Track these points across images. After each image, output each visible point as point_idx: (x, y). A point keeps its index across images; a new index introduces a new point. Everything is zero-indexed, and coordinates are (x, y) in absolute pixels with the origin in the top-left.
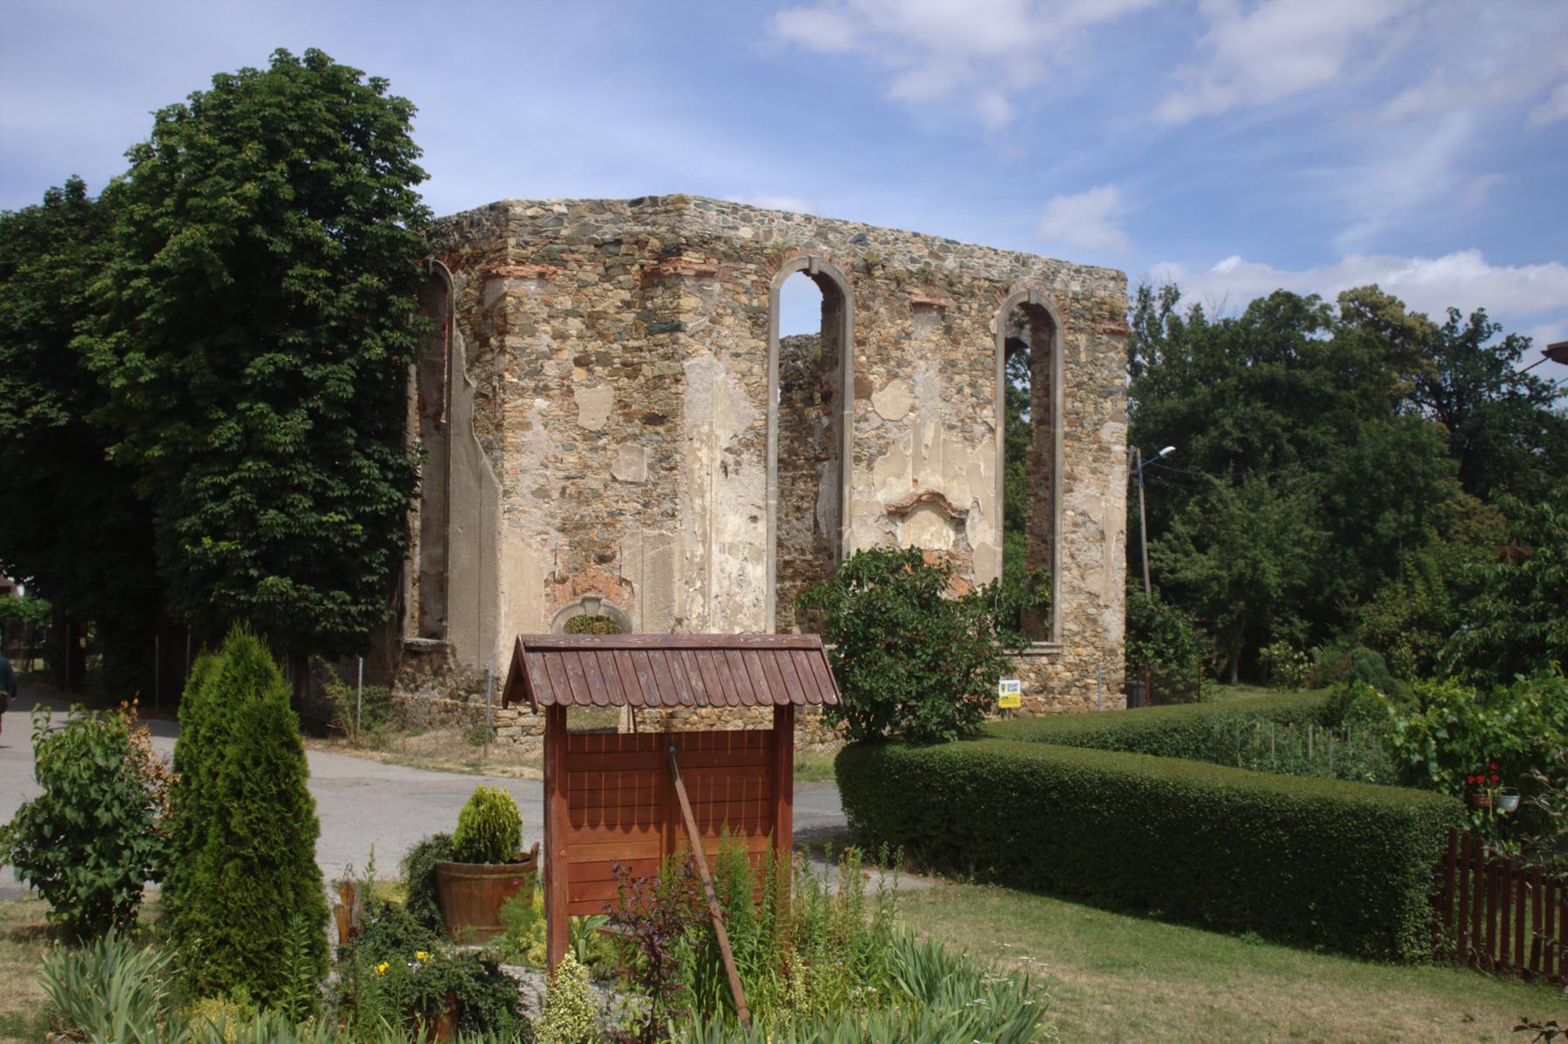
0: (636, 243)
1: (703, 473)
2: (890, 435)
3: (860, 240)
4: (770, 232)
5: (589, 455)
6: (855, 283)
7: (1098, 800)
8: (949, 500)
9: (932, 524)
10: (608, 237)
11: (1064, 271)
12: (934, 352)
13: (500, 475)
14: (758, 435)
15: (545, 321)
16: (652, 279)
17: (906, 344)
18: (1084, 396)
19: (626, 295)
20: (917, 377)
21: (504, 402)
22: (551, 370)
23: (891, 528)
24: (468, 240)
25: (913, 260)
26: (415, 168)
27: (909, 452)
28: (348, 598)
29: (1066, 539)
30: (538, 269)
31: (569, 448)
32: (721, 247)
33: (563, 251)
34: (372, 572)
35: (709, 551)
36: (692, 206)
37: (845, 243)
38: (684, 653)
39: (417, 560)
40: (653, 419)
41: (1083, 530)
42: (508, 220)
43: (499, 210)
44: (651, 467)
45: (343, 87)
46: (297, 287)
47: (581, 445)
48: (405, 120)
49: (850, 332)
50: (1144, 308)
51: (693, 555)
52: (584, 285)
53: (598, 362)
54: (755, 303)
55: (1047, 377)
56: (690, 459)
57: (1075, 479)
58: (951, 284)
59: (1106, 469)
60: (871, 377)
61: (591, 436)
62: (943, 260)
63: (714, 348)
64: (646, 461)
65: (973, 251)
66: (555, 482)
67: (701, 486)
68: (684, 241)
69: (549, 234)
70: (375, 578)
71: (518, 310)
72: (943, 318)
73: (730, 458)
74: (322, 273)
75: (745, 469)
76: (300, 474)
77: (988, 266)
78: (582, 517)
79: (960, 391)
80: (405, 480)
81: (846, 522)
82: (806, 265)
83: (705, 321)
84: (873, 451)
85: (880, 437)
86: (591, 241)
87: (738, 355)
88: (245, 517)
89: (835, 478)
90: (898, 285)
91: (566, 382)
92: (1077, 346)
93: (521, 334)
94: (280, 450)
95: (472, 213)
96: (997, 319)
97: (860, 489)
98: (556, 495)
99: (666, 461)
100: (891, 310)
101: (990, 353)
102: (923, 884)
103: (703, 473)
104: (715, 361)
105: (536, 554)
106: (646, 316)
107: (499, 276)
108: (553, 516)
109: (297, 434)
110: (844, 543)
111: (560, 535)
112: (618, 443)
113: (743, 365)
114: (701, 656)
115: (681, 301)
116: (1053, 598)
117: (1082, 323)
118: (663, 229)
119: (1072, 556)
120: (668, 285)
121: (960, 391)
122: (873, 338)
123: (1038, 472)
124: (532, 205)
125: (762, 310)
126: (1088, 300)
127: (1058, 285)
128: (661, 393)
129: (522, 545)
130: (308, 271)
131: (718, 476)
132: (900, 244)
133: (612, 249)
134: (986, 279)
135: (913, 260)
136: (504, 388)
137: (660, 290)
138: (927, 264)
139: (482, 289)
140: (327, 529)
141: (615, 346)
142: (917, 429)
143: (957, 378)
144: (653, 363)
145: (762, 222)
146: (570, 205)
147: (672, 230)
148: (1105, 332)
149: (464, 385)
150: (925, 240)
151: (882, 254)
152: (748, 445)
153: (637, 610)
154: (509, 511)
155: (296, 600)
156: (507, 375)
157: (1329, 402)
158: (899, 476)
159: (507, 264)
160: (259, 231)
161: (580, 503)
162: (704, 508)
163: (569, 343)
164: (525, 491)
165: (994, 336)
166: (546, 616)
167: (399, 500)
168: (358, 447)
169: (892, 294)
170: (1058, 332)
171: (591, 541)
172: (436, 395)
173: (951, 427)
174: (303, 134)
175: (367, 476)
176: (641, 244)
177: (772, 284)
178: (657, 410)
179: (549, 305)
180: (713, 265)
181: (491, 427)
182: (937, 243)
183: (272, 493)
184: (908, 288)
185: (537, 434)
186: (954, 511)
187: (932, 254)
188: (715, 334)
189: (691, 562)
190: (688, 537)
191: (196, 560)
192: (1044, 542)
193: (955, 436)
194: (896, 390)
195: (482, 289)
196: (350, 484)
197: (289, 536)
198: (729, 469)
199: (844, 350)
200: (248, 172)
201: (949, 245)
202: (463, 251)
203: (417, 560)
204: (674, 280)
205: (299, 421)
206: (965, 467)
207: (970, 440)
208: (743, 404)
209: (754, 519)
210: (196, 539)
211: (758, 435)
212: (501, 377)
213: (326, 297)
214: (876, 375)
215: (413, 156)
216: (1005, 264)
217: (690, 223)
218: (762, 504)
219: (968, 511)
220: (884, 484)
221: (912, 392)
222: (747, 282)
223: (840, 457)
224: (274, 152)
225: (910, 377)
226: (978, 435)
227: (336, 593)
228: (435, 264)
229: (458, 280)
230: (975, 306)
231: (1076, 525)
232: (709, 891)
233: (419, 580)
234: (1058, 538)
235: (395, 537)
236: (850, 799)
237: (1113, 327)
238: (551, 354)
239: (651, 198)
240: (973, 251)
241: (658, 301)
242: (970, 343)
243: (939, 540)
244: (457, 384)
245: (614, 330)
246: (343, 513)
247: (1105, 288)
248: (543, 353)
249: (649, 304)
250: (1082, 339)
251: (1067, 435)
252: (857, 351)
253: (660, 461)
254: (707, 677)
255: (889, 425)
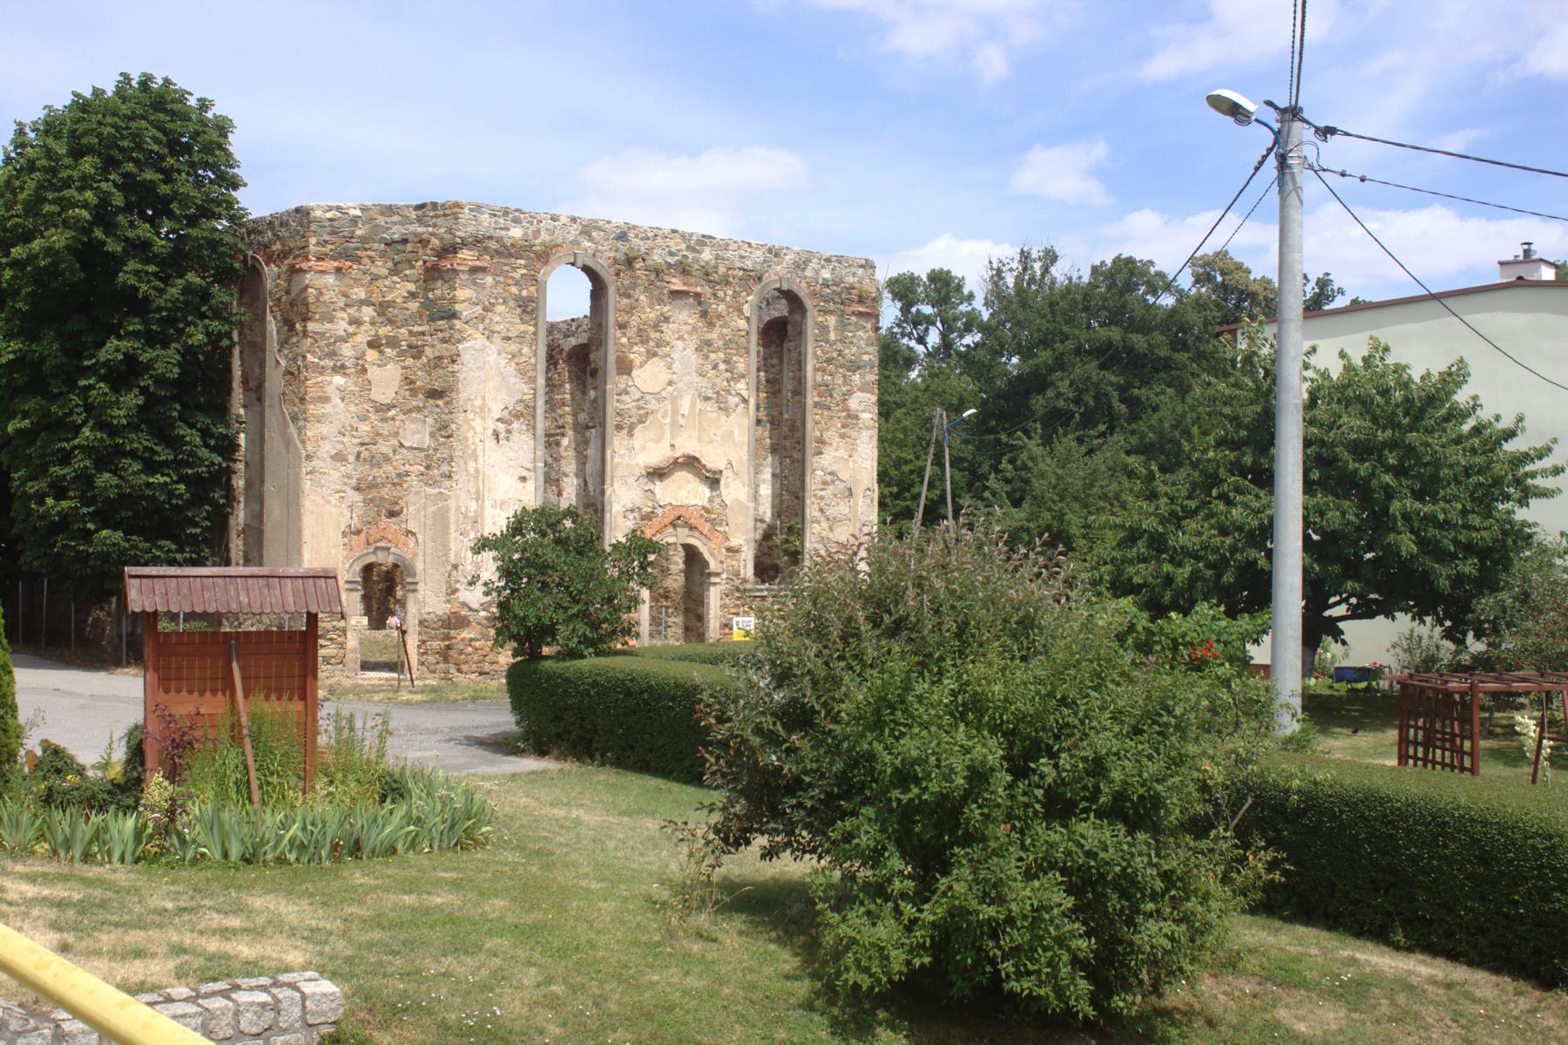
0: (420, 242)
1: (477, 440)
2: (649, 406)
3: (622, 237)
4: (539, 231)
5: (380, 424)
6: (617, 274)
7: (673, 699)
8: (704, 462)
9: (688, 482)
10: (396, 236)
11: (815, 260)
12: (691, 333)
13: (303, 442)
14: (527, 407)
15: (342, 309)
16: (433, 273)
17: (664, 327)
18: (833, 370)
19: (412, 287)
20: (675, 356)
21: (306, 379)
22: (347, 351)
23: (651, 487)
24: (279, 238)
25: (671, 254)
26: (235, 176)
27: (668, 420)
28: (173, 547)
29: (815, 495)
30: (336, 264)
31: (363, 418)
32: (493, 245)
33: (357, 249)
34: (196, 525)
35: (482, 507)
36: (466, 211)
37: (607, 240)
38: (239, 580)
39: (242, 514)
40: (434, 394)
41: (831, 487)
42: (309, 222)
43: (302, 213)
44: (432, 435)
45: (169, 107)
46: (132, 281)
47: (373, 416)
48: (226, 137)
49: (612, 318)
50: (1025, 269)
51: (467, 510)
52: (376, 278)
53: (388, 345)
54: (524, 293)
55: (800, 353)
56: (464, 428)
57: (824, 443)
58: (707, 274)
59: (854, 434)
60: (632, 356)
61: (382, 408)
62: (700, 252)
63: (487, 332)
64: (428, 429)
65: (728, 245)
66: (350, 445)
67: (474, 451)
68: (459, 241)
69: (346, 234)
70: (198, 530)
71: (318, 300)
72: (700, 304)
73: (501, 427)
74: (151, 268)
75: (515, 437)
76: (131, 442)
77: (742, 257)
78: (374, 477)
79: (715, 367)
80: (227, 447)
81: (608, 481)
82: (572, 260)
83: (479, 310)
84: (634, 420)
85: (639, 408)
86: (382, 240)
87: (508, 339)
88: (85, 480)
89: (599, 443)
90: (657, 275)
91: (360, 362)
92: (827, 327)
93: (321, 320)
94: (115, 422)
95: (282, 214)
96: (749, 304)
97: (622, 452)
98: (352, 459)
99: (444, 430)
100: (650, 297)
101: (743, 333)
102: (567, 766)
103: (477, 440)
104: (487, 343)
105: (334, 510)
106: (428, 305)
107: (301, 270)
108: (349, 477)
109: (129, 409)
110: (606, 500)
111: (356, 493)
112: (405, 414)
113: (514, 347)
114: (250, 581)
115: (457, 293)
116: (803, 547)
117: (831, 306)
118: (442, 230)
119: (822, 511)
120: (447, 278)
121: (715, 367)
122: (634, 321)
123: (792, 437)
124: (330, 209)
125: (530, 299)
126: (838, 286)
127: (808, 273)
128: (441, 371)
129: (322, 502)
130: (139, 266)
131: (490, 442)
132: (659, 240)
133: (400, 247)
134: (740, 269)
135: (671, 254)
136: (306, 367)
137: (439, 283)
138: (684, 256)
139: (289, 281)
140: (155, 489)
141: (402, 331)
142: (674, 400)
143: (713, 356)
144: (433, 346)
145: (531, 223)
146: (364, 209)
147: (450, 231)
148: (853, 313)
149: (277, 361)
150: (683, 236)
151: (643, 249)
152: (518, 416)
153: (421, 557)
154: (311, 473)
155: (127, 550)
156: (309, 356)
157: (1167, 365)
158: (657, 442)
159: (309, 260)
160: (98, 233)
161: (372, 466)
162: (477, 471)
163: (363, 328)
164: (325, 456)
165: (748, 319)
166: (343, 563)
167: (220, 464)
168: (182, 419)
169: (652, 283)
170: (809, 314)
171: (382, 498)
172: (257, 371)
173: (707, 399)
174: (132, 150)
175: (190, 443)
176: (424, 243)
177: (540, 277)
178: (437, 386)
179: (345, 295)
180: (485, 261)
181: (297, 401)
182: (695, 238)
183: (105, 459)
184: (667, 278)
185: (335, 407)
186: (708, 471)
187: (689, 248)
188: (487, 321)
189: (466, 516)
190: (463, 496)
191: (43, 517)
192: (797, 498)
193: (710, 407)
194: (655, 366)
195: (289, 281)
196: (174, 450)
197: (121, 495)
198: (501, 436)
199: (606, 333)
200: (85, 182)
201: (705, 240)
202: (274, 248)
203: (242, 514)
204: (450, 275)
205: (132, 399)
206: (719, 433)
207: (725, 410)
208: (513, 380)
209: (523, 479)
210: (41, 500)
211: (527, 407)
212: (304, 357)
213: (155, 288)
214: (636, 354)
215: (231, 167)
216: (759, 255)
217: (465, 226)
218: (530, 466)
219: (721, 472)
220: (643, 448)
221: (670, 368)
222: (517, 275)
223: (603, 425)
224: (109, 164)
225: (668, 355)
226: (733, 406)
227: (162, 543)
228: (253, 257)
229: (270, 271)
230: (730, 292)
231: (825, 483)
232: (245, 731)
233: (244, 531)
234: (807, 495)
235: (216, 496)
236: (518, 704)
237: (861, 309)
238: (347, 338)
239: (432, 203)
240: (728, 245)
241: (438, 292)
242: (726, 325)
243: (695, 497)
244: (270, 363)
245: (401, 317)
246: (168, 475)
247: (854, 275)
248: (341, 336)
249: (431, 295)
250: (832, 321)
251: (816, 405)
252: (618, 334)
253: (440, 430)
254: (251, 594)
255: (648, 397)
